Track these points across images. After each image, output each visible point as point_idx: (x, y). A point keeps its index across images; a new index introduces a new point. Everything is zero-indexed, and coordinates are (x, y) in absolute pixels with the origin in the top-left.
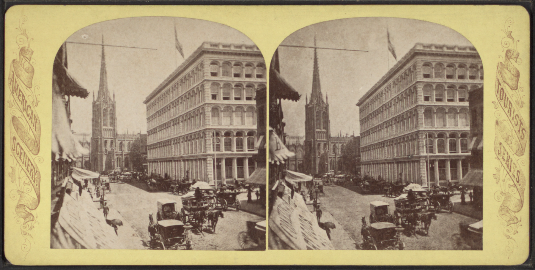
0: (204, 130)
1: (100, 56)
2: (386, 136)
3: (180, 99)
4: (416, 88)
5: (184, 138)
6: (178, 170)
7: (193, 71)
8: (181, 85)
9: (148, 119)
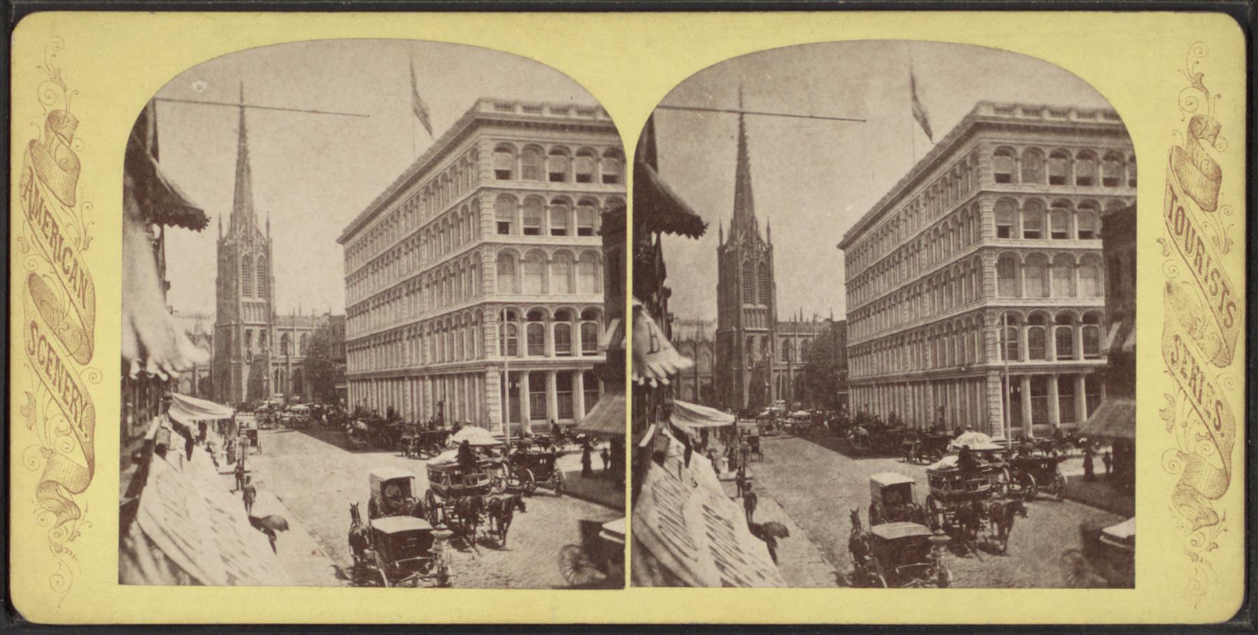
0: (480, 305)
1: (235, 131)
2: (907, 321)
3: (423, 232)
4: (978, 207)
5: (432, 325)
6: (418, 399)
7: (453, 168)
8: (425, 200)
9: (348, 280)
